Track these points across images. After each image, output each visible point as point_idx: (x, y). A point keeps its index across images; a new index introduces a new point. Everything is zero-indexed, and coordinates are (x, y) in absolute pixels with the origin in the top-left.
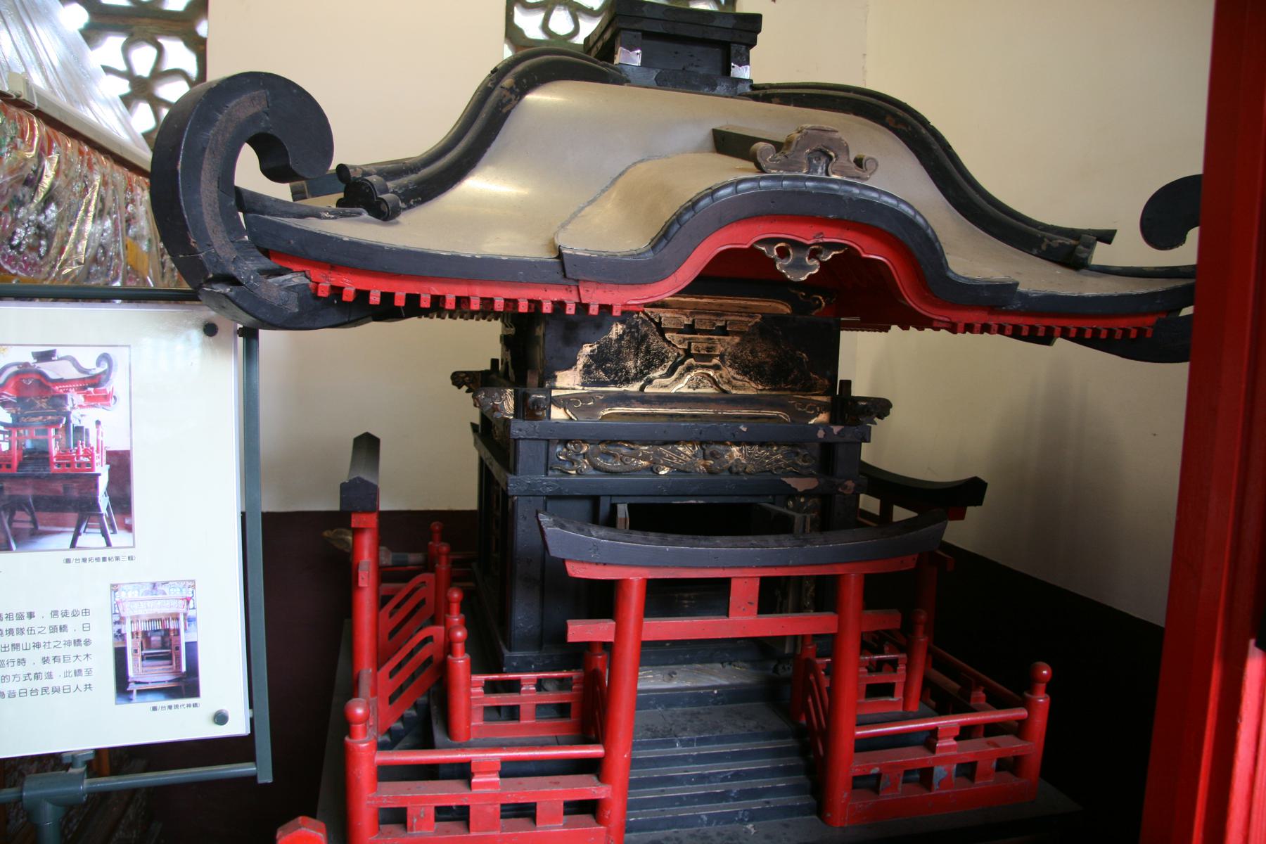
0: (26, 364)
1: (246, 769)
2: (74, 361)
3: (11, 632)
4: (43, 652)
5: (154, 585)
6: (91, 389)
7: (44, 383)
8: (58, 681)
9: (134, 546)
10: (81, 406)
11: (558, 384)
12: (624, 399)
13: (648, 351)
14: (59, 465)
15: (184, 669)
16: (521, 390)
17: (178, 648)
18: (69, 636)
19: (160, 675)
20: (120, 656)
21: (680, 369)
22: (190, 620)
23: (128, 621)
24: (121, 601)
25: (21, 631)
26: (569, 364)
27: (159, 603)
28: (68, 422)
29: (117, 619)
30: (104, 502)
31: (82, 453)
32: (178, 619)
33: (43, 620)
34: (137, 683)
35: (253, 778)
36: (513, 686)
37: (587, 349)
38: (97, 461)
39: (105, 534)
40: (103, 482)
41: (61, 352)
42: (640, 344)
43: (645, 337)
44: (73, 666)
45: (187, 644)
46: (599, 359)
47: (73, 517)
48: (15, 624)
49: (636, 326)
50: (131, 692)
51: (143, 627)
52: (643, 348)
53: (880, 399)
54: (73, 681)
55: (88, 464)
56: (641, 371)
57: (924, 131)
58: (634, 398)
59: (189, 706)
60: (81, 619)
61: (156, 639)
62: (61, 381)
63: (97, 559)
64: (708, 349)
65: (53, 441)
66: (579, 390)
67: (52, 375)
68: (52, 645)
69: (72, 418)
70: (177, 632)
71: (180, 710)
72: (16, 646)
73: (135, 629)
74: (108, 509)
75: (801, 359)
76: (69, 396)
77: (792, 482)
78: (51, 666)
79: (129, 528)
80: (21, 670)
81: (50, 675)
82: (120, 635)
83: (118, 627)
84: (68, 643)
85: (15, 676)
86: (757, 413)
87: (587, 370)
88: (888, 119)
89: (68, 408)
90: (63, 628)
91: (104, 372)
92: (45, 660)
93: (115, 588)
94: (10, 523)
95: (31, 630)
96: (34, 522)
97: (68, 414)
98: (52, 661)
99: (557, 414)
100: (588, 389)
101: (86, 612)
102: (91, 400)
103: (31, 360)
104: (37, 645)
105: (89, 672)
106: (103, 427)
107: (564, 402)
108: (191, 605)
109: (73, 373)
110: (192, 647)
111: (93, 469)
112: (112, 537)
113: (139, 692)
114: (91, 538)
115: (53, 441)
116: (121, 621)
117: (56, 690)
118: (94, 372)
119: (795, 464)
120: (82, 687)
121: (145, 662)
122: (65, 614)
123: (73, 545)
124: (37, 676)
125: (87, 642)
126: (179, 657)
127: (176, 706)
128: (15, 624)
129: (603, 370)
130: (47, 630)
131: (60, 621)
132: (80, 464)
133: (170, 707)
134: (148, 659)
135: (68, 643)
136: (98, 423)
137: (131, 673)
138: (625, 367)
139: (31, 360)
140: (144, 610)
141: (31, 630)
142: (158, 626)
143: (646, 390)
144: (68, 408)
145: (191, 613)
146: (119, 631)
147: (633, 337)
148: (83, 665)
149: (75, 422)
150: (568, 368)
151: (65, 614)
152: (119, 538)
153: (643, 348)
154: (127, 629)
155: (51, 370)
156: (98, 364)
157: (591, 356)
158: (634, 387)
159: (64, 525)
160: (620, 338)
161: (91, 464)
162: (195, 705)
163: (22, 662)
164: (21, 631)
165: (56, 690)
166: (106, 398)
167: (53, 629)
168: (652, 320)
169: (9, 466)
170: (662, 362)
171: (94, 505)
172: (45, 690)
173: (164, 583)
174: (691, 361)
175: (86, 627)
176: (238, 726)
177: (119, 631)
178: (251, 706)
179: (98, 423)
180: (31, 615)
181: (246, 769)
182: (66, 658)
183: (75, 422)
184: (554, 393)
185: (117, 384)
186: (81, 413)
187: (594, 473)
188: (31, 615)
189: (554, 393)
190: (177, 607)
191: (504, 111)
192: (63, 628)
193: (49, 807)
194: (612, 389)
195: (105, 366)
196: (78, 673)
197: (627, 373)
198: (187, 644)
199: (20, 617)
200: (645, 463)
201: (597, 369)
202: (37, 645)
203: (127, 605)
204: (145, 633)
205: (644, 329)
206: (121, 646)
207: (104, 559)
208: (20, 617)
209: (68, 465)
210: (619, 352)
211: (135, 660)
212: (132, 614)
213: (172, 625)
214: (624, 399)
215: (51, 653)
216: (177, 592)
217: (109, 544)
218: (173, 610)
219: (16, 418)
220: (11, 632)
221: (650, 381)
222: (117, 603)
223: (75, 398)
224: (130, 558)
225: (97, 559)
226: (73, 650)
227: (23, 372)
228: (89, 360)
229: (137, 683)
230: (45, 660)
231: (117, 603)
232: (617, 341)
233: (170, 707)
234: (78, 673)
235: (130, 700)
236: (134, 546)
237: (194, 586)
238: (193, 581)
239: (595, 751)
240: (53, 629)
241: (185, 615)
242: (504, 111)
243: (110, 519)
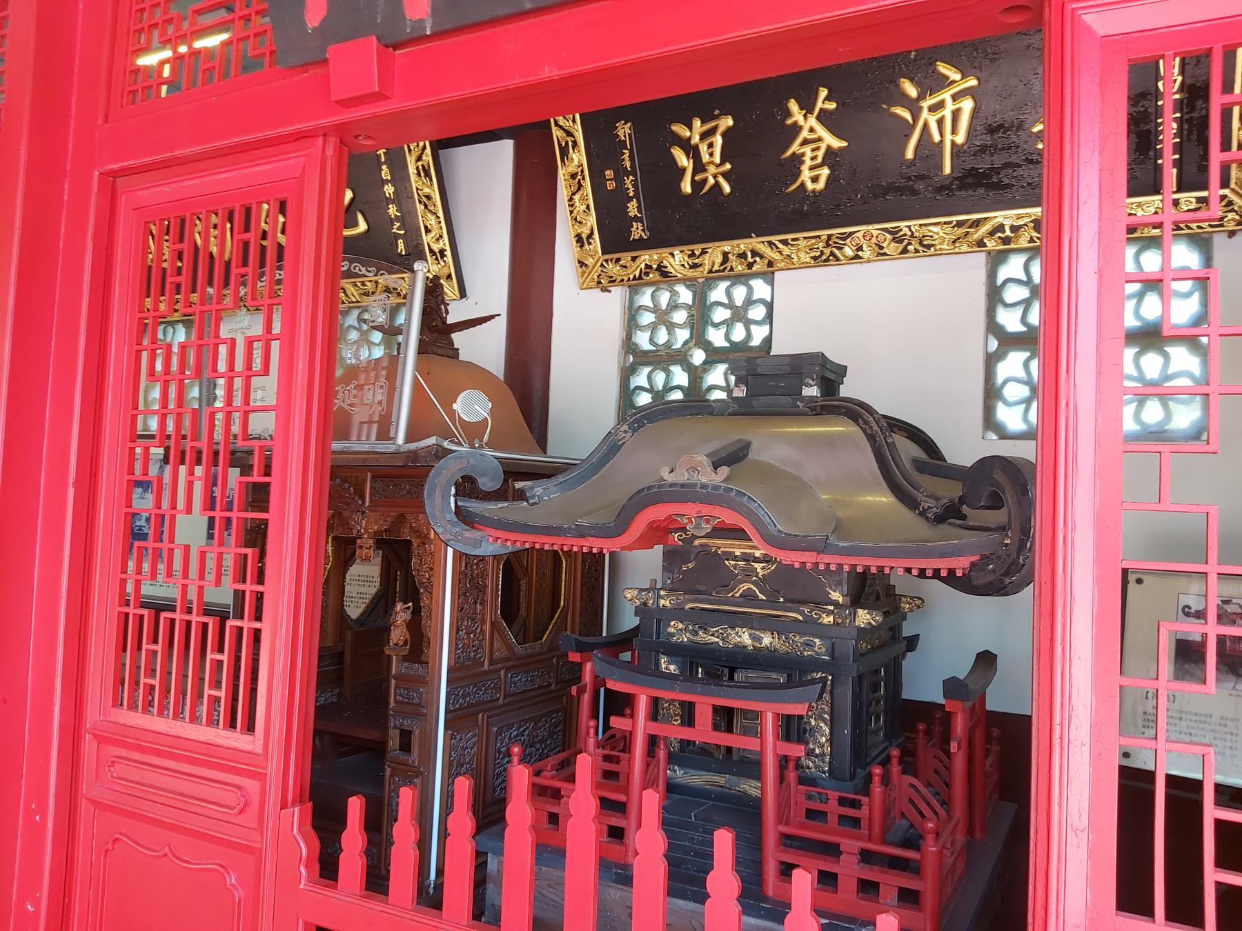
18: (1228, 730)
41: (1234, 601)
48: (1203, 719)
90: (1226, 726)
123: (1234, 688)
131: (1223, 722)
167: (1220, 725)
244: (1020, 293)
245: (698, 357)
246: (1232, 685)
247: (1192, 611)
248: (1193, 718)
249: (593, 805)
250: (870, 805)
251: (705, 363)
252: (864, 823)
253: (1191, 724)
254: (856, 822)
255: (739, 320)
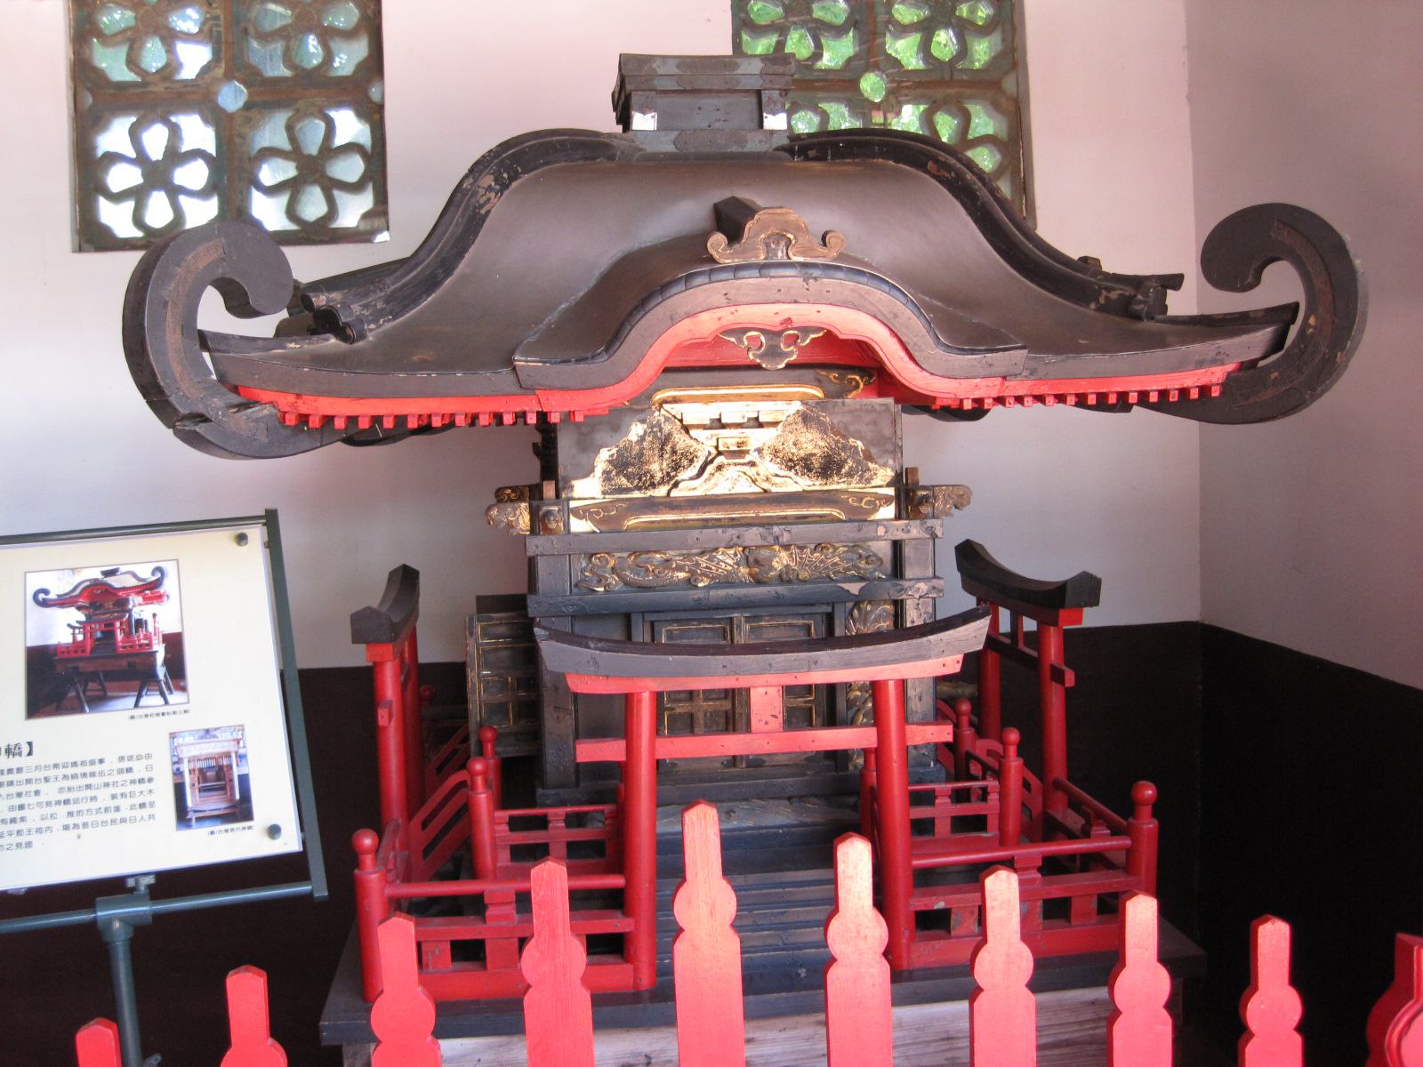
0: (96, 580)
1: (304, 888)
2: (135, 576)
3: (84, 775)
4: (112, 790)
5: (207, 731)
6: (148, 592)
7: (109, 591)
8: (125, 813)
9: (188, 702)
10: (140, 605)
11: (576, 494)
12: (651, 505)
13: (674, 452)
14: (124, 647)
15: (238, 797)
16: (535, 503)
17: (231, 780)
18: (135, 776)
19: (215, 804)
20: (179, 790)
21: (710, 469)
22: (241, 757)
23: (186, 761)
24: (179, 745)
25: (93, 774)
26: (588, 472)
27: (213, 745)
28: (130, 616)
29: (176, 760)
30: (161, 672)
31: (142, 637)
32: (230, 757)
33: (112, 764)
34: (195, 811)
35: (310, 895)
36: (542, 823)
37: (604, 454)
38: (155, 641)
39: (162, 694)
40: (160, 657)
41: (123, 569)
42: (664, 444)
43: (668, 437)
44: (138, 801)
45: (239, 776)
46: (621, 464)
47: (137, 683)
48: (88, 769)
49: (659, 425)
50: (190, 820)
51: (199, 765)
52: (668, 448)
53: (1203, 272)
54: (139, 813)
55: (148, 645)
56: (668, 474)
57: (969, 176)
58: (661, 504)
59: (244, 828)
60: (144, 762)
61: (210, 774)
62: (124, 589)
63: (158, 715)
64: (739, 444)
65: (118, 631)
66: (600, 498)
67: (117, 585)
68: (119, 784)
69: (133, 613)
70: (230, 767)
71: (236, 834)
72: (89, 787)
73: (192, 767)
74: (165, 676)
75: (856, 448)
76: (130, 598)
77: (846, 586)
78: (119, 802)
79: (184, 689)
80: (93, 806)
81: (117, 809)
82: (178, 773)
83: (176, 766)
84: (133, 782)
85: (88, 811)
86: (805, 512)
87: (607, 476)
88: (930, 164)
89: (130, 607)
90: (129, 770)
91: (158, 580)
92: (114, 797)
93: (173, 736)
94: (84, 692)
95: (101, 774)
96: (104, 689)
97: (130, 611)
98: (119, 797)
99: (579, 526)
100: (609, 498)
101: (149, 756)
102: (148, 600)
103: (100, 576)
104: (107, 785)
105: (152, 804)
106: (160, 618)
107: (581, 513)
108: (241, 744)
109: (133, 582)
110: (244, 780)
111: (151, 648)
112: (170, 698)
113: (198, 819)
114: (152, 700)
115: (119, 630)
116: (180, 761)
117: (123, 821)
118: (150, 580)
119: (856, 567)
120: (146, 817)
121: (202, 794)
122: (131, 758)
123: (136, 705)
124: (107, 810)
125: (150, 780)
126: (232, 788)
127: (232, 830)
128: (88, 769)
129: (625, 476)
130: (115, 772)
131: (125, 765)
132: (140, 646)
133: (227, 831)
134: (205, 790)
135: (133, 782)
136: (154, 615)
137: (189, 803)
138: (649, 471)
139: (100, 576)
140: (197, 750)
141: (101, 774)
142: (213, 763)
143: (672, 494)
144: (130, 607)
145: (242, 751)
146: (178, 769)
147: (655, 436)
148: (146, 799)
149: (136, 616)
150: (586, 475)
151: (131, 758)
152: (176, 697)
153: (668, 448)
154: (185, 767)
155: (115, 582)
156: (153, 574)
157: (610, 462)
158: (661, 491)
159: (128, 690)
160: (642, 439)
161: (150, 645)
162: (250, 828)
163: (94, 799)
164: (93, 774)
165: (123, 821)
166: (159, 598)
167: (121, 771)
168: (675, 417)
169: (83, 651)
170: (691, 461)
171: (154, 675)
172: (113, 821)
173: (216, 729)
174: (721, 459)
175: (149, 768)
176: (290, 842)
177: (178, 769)
178: (302, 830)
179: (154, 615)
180: (101, 761)
181: (304, 888)
182: (132, 794)
183: (136, 616)
184: (573, 504)
185: (169, 586)
186: (140, 609)
187: (625, 589)
188: (101, 761)
189: (573, 504)
190: (231, 747)
191: (483, 211)
192: (129, 770)
193: (117, 925)
194: (636, 494)
195: (159, 575)
196: (142, 806)
197: (652, 477)
198: (239, 776)
199: (92, 763)
200: (682, 575)
201: (617, 474)
202: (107, 785)
203: (184, 749)
204: (201, 770)
205: (667, 428)
206: (180, 781)
207: (163, 714)
208: (92, 763)
209: (132, 647)
210: (641, 454)
211: (193, 793)
212: (188, 755)
213: (225, 762)
214: (651, 505)
215: (118, 791)
216: (228, 735)
217: (166, 702)
218: (225, 750)
219: (89, 617)
220: (84, 775)
221: (676, 485)
222: (176, 747)
223: (134, 600)
224: (186, 712)
225: (158, 715)
226: (137, 787)
227: (95, 584)
228: (146, 573)
229: (195, 811)
230: (114, 797)
231: (176, 747)
232: (637, 442)
233: (227, 831)
234: (142, 806)
235: (189, 826)
236: (188, 702)
237: (243, 730)
238: (242, 726)
239: (617, 881)
240: (121, 771)
241: (236, 753)
242: (483, 211)
243: (167, 683)
244: (944, 42)
245: (232, 97)
246: (132, 701)
247: (52, 596)
248: (70, 771)
249: (576, 953)
250: (1003, 795)
251: (248, 106)
252: (993, 822)
253: (66, 784)
254: (978, 823)
255: (310, 30)
